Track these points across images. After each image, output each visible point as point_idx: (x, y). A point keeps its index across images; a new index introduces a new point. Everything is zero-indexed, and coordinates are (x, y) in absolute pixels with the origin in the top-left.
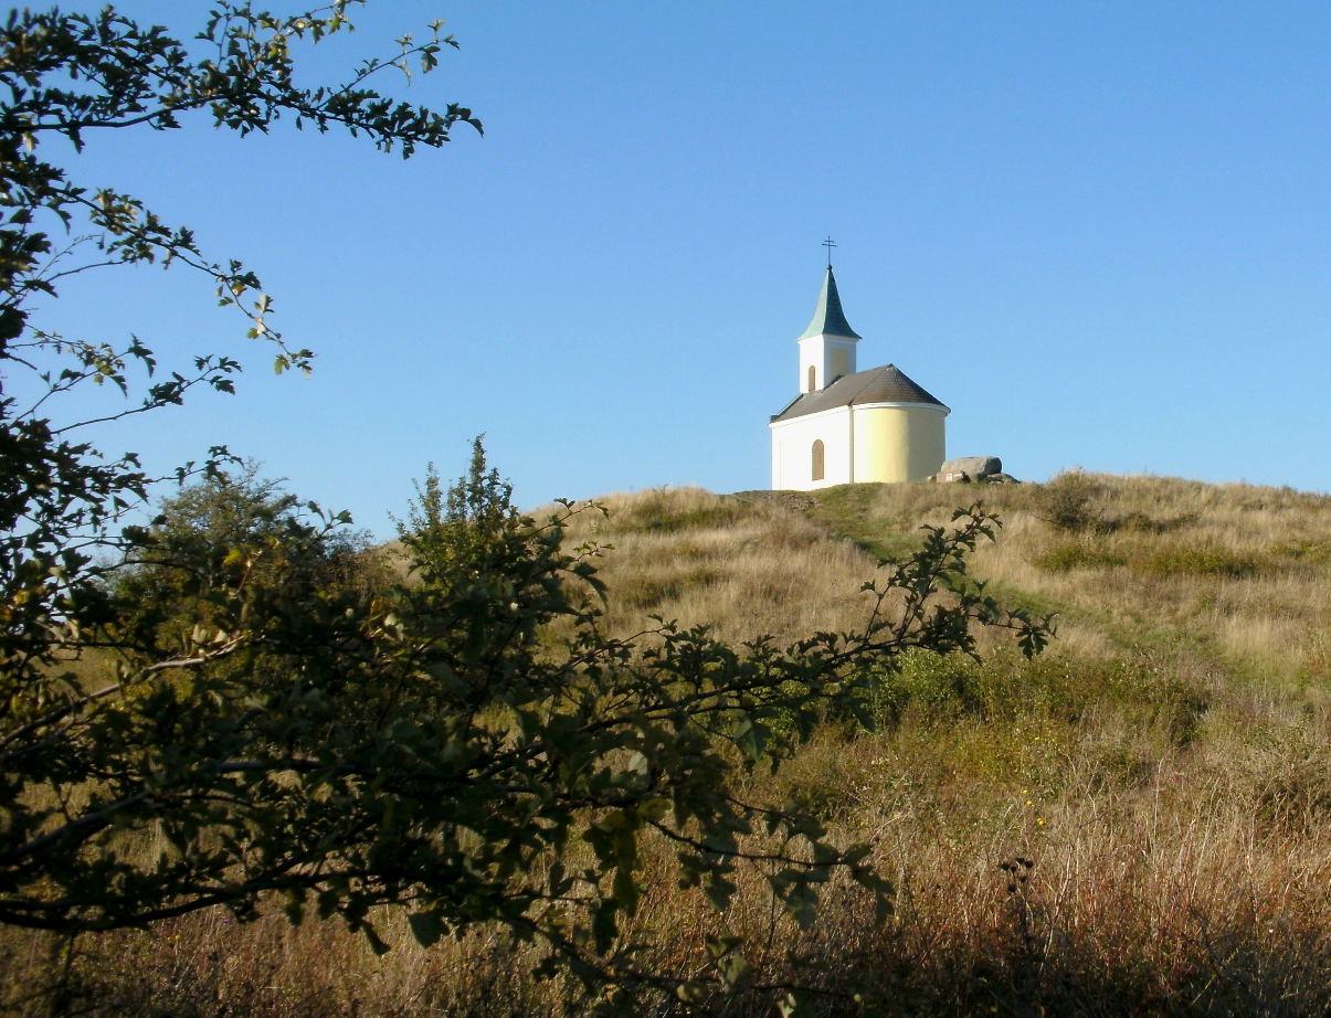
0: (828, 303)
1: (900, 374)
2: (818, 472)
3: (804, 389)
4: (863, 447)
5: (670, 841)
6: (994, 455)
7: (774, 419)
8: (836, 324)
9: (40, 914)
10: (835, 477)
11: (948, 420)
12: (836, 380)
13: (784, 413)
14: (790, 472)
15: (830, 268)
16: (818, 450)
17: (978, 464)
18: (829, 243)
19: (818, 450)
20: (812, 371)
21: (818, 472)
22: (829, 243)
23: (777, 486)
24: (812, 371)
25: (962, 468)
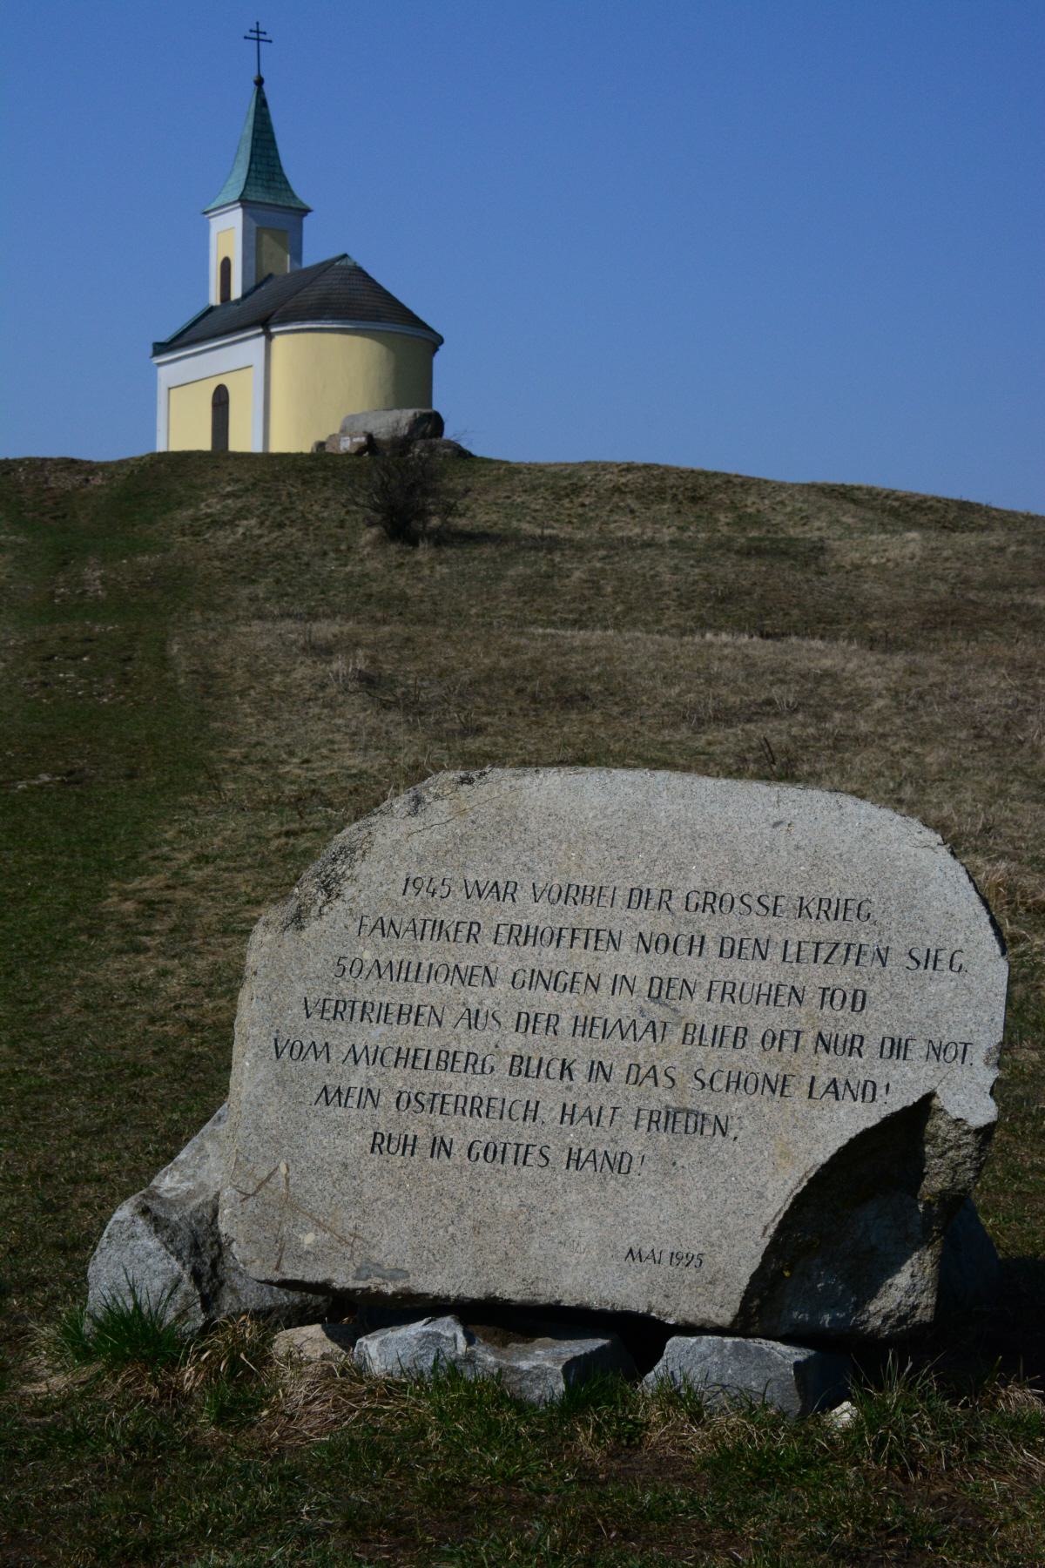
1: (359, 272)
3: (214, 299)
7: (161, 348)
15: (259, 82)
16: (221, 400)
18: (258, 36)
19: (221, 400)
20: (226, 265)
22: (258, 36)
24: (226, 265)
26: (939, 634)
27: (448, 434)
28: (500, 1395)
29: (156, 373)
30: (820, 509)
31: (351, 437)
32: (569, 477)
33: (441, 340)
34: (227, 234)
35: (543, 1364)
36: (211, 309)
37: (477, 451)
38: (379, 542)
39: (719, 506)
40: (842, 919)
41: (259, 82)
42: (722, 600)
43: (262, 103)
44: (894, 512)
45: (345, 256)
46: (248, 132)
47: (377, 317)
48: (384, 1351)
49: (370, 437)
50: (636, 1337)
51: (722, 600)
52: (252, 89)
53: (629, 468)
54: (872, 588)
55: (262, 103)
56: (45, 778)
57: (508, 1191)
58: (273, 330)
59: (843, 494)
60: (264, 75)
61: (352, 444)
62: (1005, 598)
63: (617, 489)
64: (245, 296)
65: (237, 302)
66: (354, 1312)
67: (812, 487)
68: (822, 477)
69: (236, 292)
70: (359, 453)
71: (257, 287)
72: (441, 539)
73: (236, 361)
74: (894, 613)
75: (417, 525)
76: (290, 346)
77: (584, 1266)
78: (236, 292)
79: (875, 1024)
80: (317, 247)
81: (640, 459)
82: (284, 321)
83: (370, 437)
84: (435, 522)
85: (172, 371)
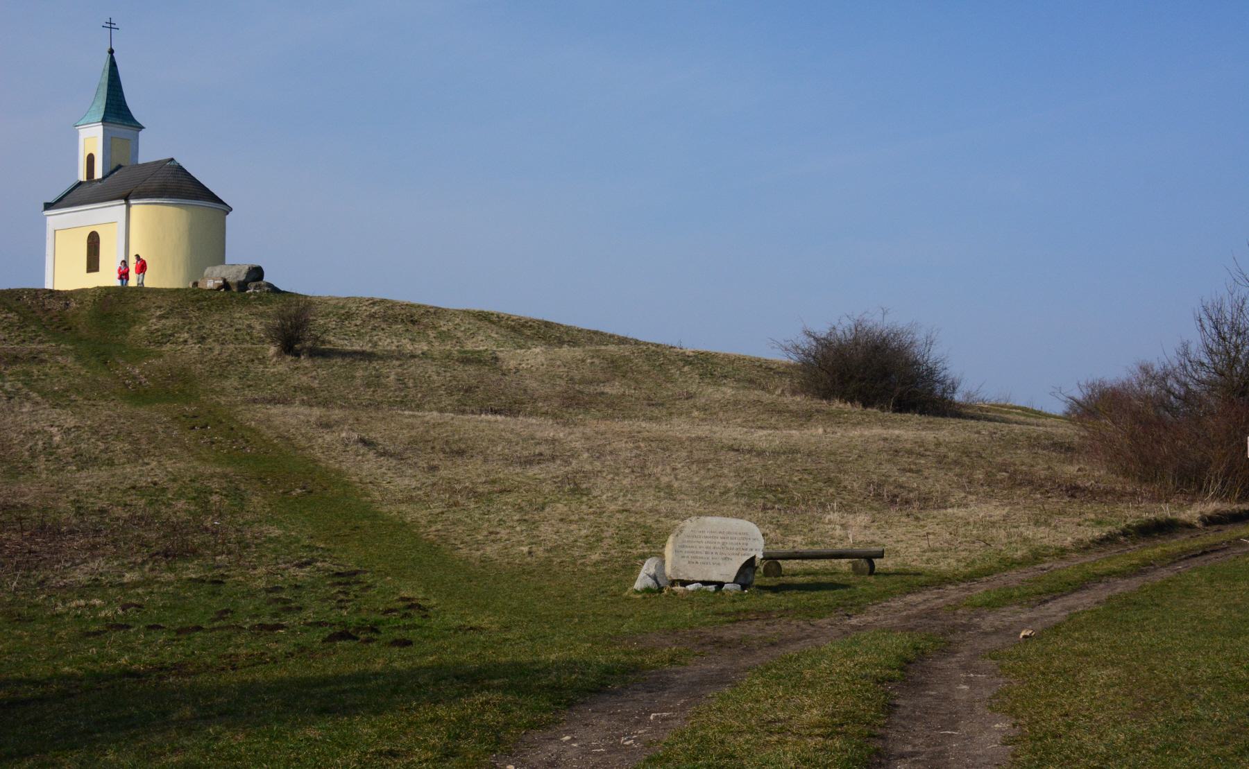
0: (109, 90)
1: (180, 168)
2: (93, 264)
3: (82, 176)
4: (136, 243)
5: (124, 660)
6: (256, 263)
7: (48, 206)
8: (117, 111)
9: (752, 616)
10: (107, 277)
11: (229, 218)
12: (116, 169)
13: (60, 200)
14: (66, 272)
15: (111, 52)
16: (93, 242)
17: (239, 272)
18: (111, 25)
19: (93, 242)
20: (91, 159)
21: (93, 264)
22: (111, 25)
23: (48, 286)
24: (91, 159)
25: (223, 275)
26: (571, 410)
27: (266, 279)
28: (706, 591)
30: (479, 329)
32: (343, 307)
35: (712, 588)
36: (80, 183)
37: (282, 289)
38: (278, 354)
39: (426, 326)
40: (745, 536)
41: (111, 52)
42: (466, 391)
44: (513, 329)
46: (105, 81)
47: (197, 198)
48: (690, 587)
49: (225, 280)
50: (720, 585)
51: (466, 391)
52: (107, 55)
53: (374, 303)
54: (532, 384)
55: (113, 65)
56: (299, 491)
57: (706, 568)
58: (132, 202)
59: (484, 317)
62: (591, 389)
63: (372, 316)
64: (104, 178)
65: (99, 180)
66: (684, 583)
67: (467, 313)
68: (476, 307)
69: (98, 174)
70: (218, 289)
71: (112, 172)
72: (314, 353)
73: (107, 218)
74: (546, 399)
75: (297, 346)
76: (140, 209)
77: (715, 577)
78: (98, 174)
79: (749, 547)
80: (150, 150)
81: (378, 296)
82: (139, 196)
83: (225, 280)
84: (309, 344)
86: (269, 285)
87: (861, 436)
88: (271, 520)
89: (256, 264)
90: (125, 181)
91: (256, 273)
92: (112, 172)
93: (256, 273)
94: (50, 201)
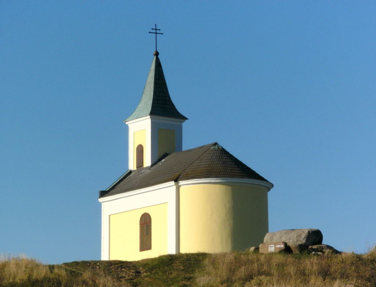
1: (224, 152)
3: (132, 166)
7: (103, 194)
8: (163, 107)
11: (271, 195)
14: (119, 243)
15: (157, 54)
16: (146, 222)
18: (156, 31)
19: (146, 222)
20: (140, 150)
22: (156, 31)
23: (105, 257)
24: (140, 150)
27: (325, 242)
29: (99, 207)
31: (275, 244)
33: (272, 186)
34: (140, 131)
36: (131, 172)
41: (157, 54)
43: (158, 65)
45: (216, 144)
49: (286, 244)
55: (158, 65)
60: (158, 51)
61: (276, 248)
64: (152, 166)
65: (147, 168)
73: (158, 199)
78: (147, 162)
82: (188, 177)
83: (286, 244)
85: (110, 205)
86: (329, 247)
87: (191, 274)
88: (168, 273)
89: (315, 228)
90: (171, 162)
91: (315, 237)
92: (160, 160)
93: (315, 237)
94: (104, 189)
